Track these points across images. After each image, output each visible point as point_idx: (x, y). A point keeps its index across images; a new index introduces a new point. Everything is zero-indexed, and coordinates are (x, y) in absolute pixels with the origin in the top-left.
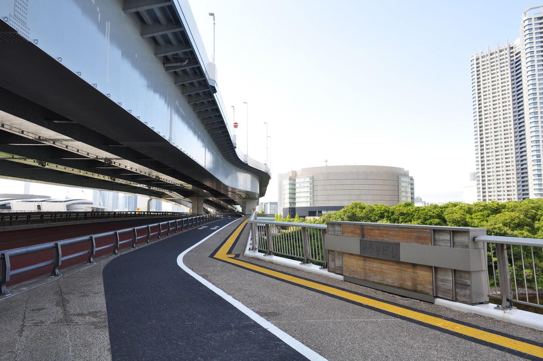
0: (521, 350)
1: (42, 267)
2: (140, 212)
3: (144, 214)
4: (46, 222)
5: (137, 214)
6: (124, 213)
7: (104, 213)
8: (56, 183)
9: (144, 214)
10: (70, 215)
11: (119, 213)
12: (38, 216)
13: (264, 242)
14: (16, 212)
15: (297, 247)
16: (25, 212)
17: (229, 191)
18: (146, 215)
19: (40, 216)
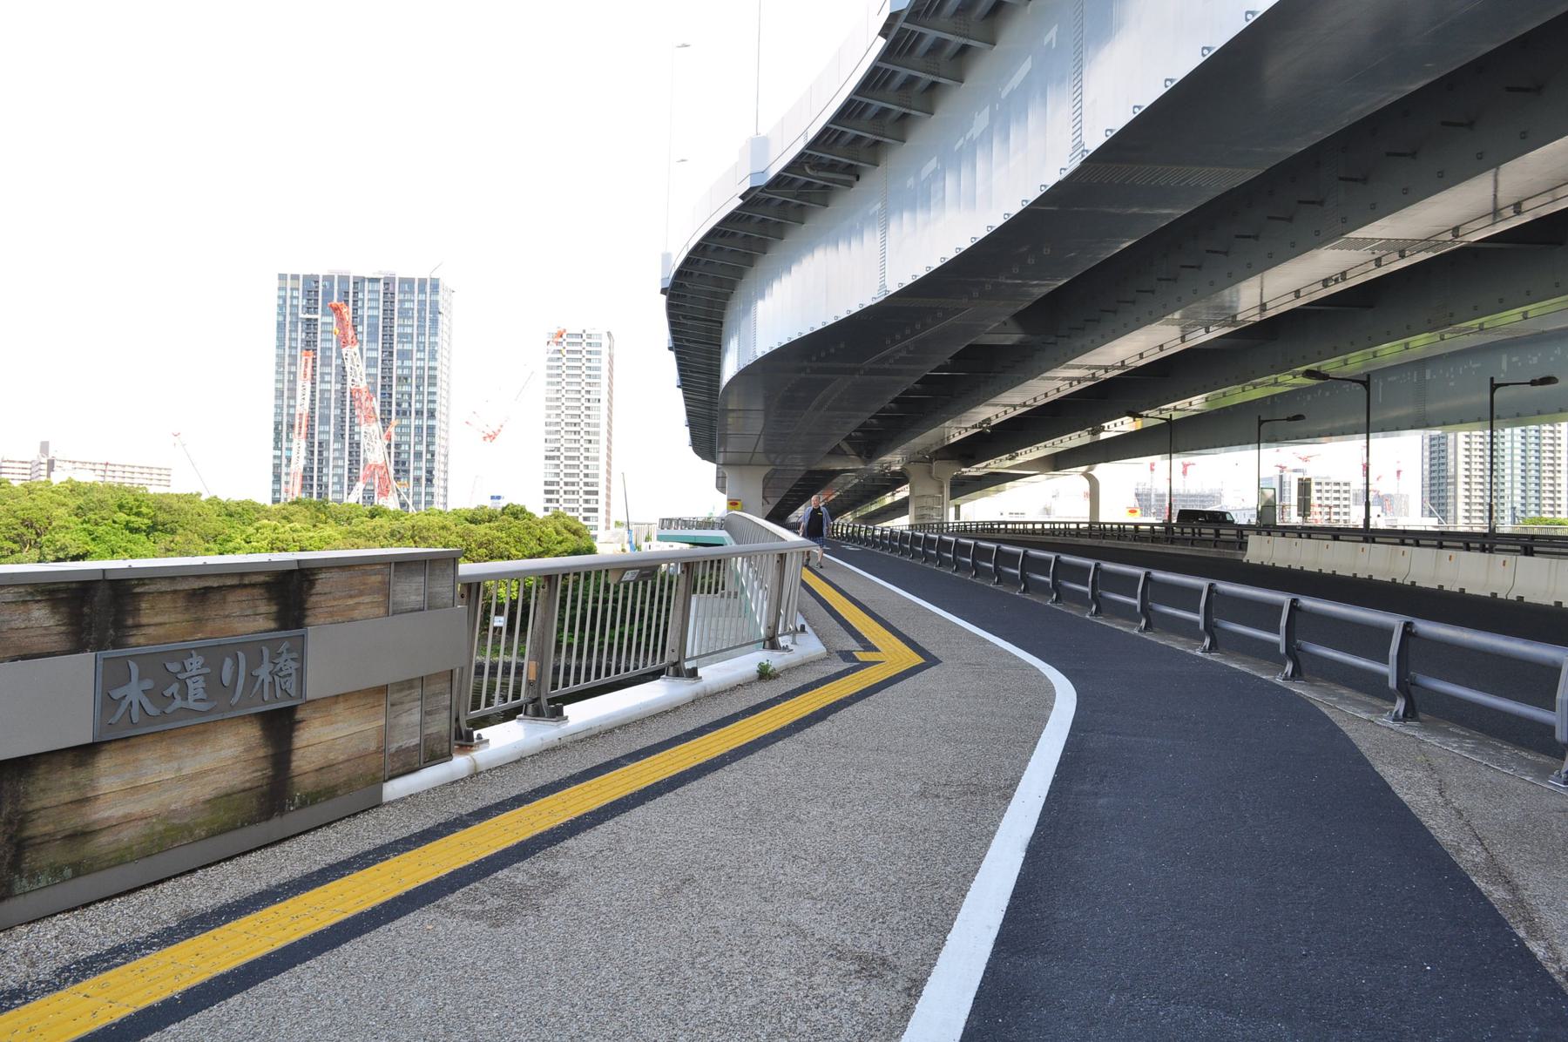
0: (704, 740)
1: (1122, 594)
2: (1054, 523)
3: (1153, 530)
4: (1245, 538)
5: (1047, 529)
6: (1017, 526)
7: (1104, 527)
8: (1231, 445)
9: (1153, 530)
10: (1200, 530)
11: (1119, 527)
12: (1225, 537)
13: (582, 629)
14: (1402, 528)
15: (623, 636)
16: (1407, 528)
17: (1492, 530)
18: (1002, 532)
19: (1222, 537)
